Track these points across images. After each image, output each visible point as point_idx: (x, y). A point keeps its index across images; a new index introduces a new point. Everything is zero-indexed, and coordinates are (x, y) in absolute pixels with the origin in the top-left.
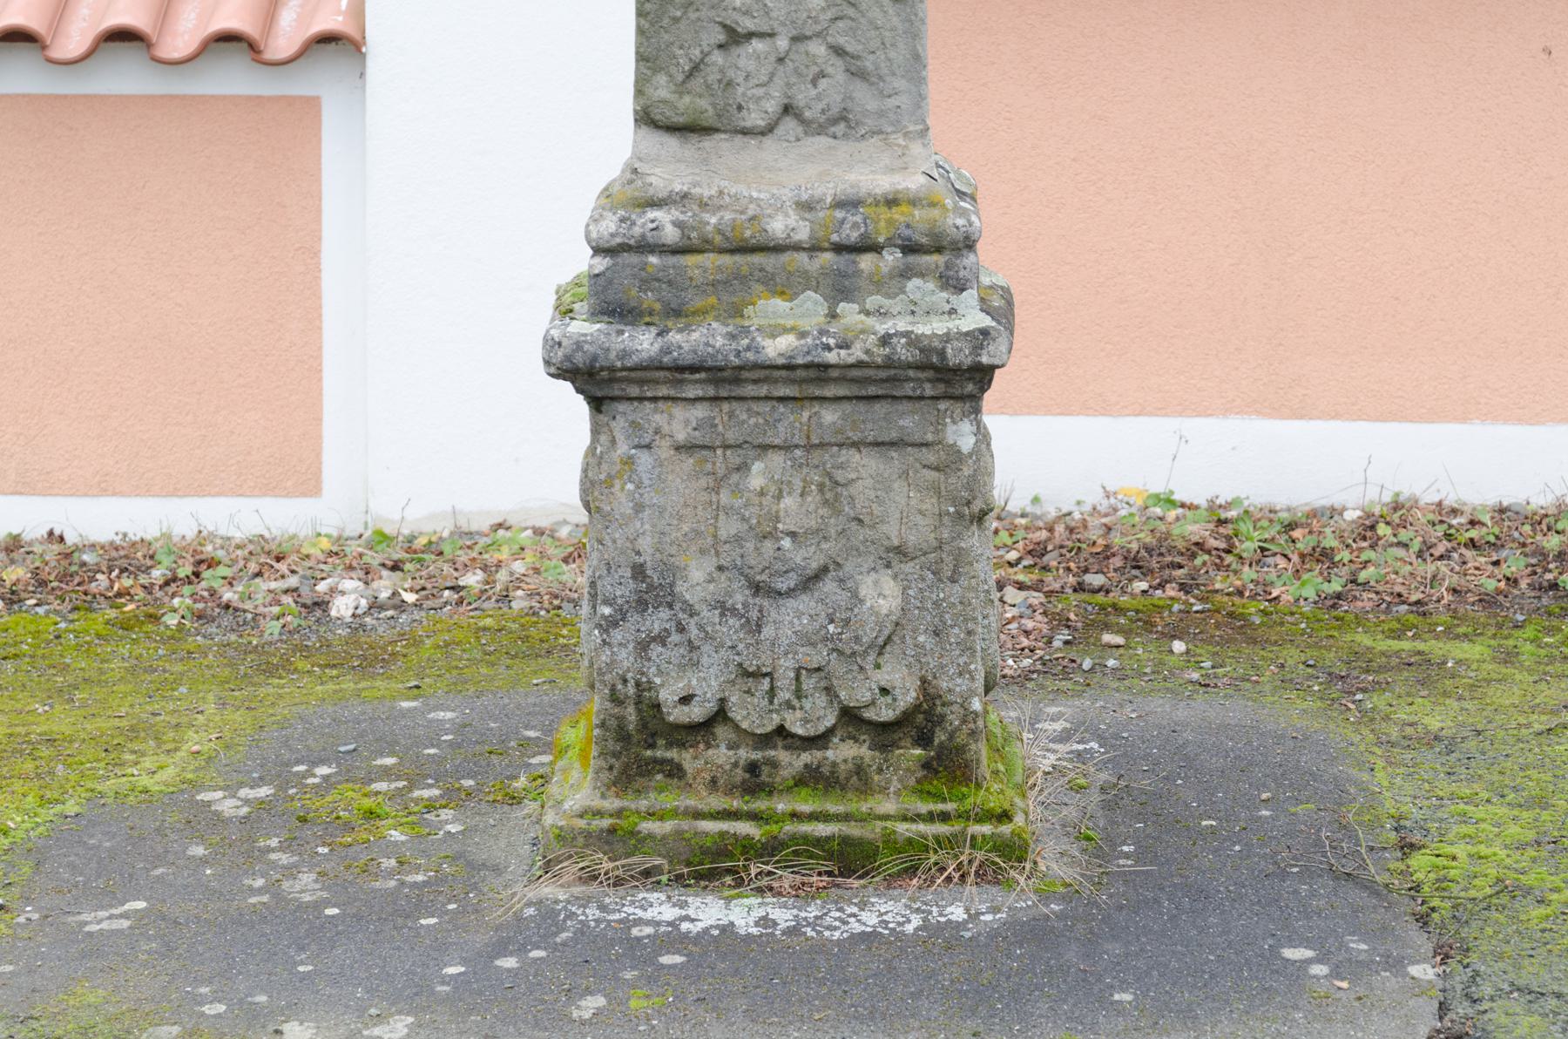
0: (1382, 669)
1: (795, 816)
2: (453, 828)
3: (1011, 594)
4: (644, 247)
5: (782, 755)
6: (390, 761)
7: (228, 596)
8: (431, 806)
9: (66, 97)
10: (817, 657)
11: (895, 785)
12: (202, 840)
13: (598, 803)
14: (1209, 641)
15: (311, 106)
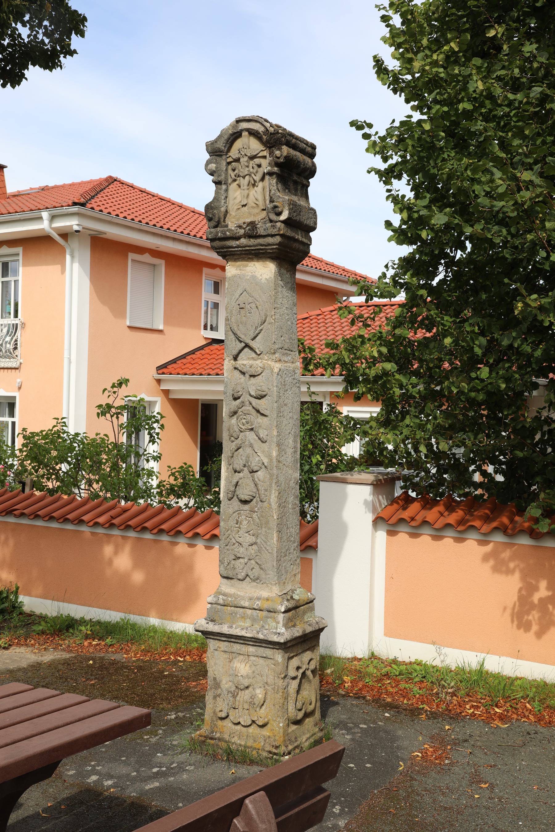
15: (311, 560)
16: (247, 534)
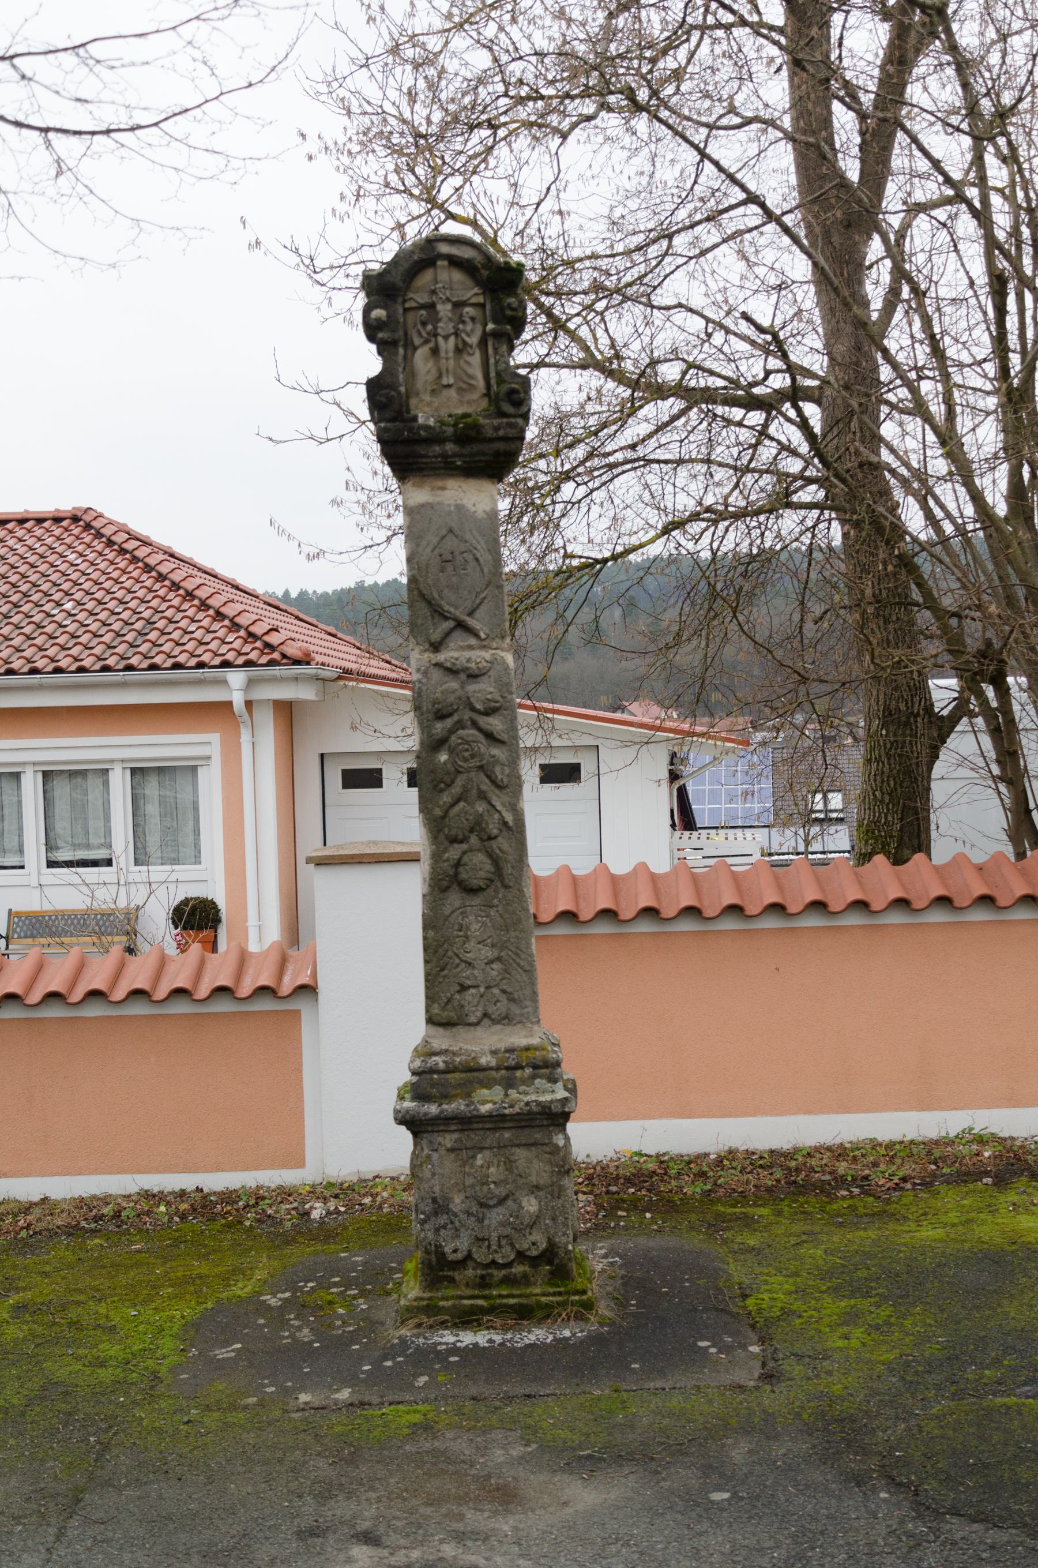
0: (730, 1221)
1: (501, 1296)
2: (364, 1307)
3: (581, 1197)
4: (432, 1071)
5: (495, 1272)
6: (337, 1279)
7: (269, 1212)
8: (354, 1297)
9: (45, 792)
10: (508, 1231)
11: (540, 1282)
12: (263, 1317)
13: (421, 1295)
14: (660, 1212)
15: (298, 1012)
16: (480, 946)
